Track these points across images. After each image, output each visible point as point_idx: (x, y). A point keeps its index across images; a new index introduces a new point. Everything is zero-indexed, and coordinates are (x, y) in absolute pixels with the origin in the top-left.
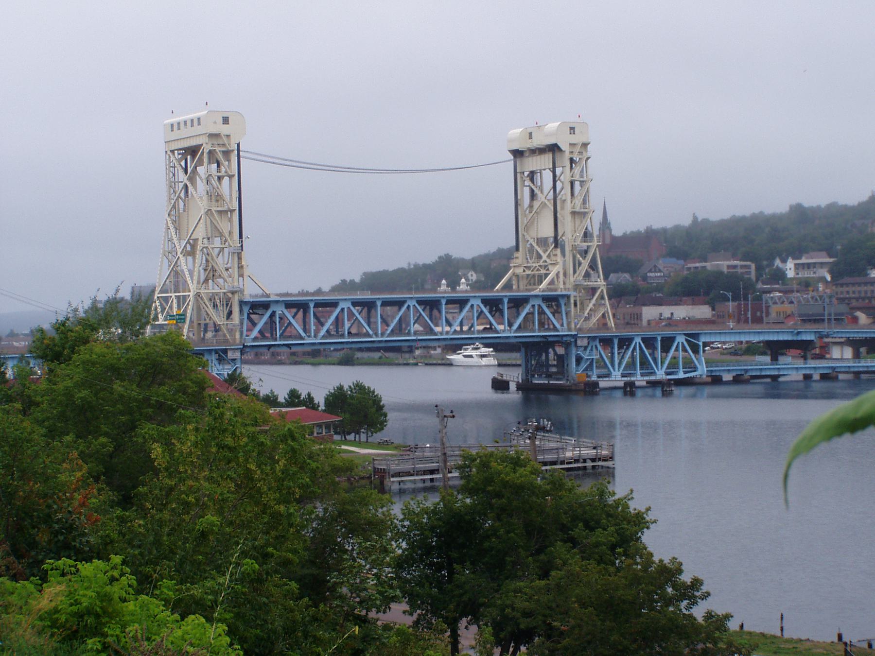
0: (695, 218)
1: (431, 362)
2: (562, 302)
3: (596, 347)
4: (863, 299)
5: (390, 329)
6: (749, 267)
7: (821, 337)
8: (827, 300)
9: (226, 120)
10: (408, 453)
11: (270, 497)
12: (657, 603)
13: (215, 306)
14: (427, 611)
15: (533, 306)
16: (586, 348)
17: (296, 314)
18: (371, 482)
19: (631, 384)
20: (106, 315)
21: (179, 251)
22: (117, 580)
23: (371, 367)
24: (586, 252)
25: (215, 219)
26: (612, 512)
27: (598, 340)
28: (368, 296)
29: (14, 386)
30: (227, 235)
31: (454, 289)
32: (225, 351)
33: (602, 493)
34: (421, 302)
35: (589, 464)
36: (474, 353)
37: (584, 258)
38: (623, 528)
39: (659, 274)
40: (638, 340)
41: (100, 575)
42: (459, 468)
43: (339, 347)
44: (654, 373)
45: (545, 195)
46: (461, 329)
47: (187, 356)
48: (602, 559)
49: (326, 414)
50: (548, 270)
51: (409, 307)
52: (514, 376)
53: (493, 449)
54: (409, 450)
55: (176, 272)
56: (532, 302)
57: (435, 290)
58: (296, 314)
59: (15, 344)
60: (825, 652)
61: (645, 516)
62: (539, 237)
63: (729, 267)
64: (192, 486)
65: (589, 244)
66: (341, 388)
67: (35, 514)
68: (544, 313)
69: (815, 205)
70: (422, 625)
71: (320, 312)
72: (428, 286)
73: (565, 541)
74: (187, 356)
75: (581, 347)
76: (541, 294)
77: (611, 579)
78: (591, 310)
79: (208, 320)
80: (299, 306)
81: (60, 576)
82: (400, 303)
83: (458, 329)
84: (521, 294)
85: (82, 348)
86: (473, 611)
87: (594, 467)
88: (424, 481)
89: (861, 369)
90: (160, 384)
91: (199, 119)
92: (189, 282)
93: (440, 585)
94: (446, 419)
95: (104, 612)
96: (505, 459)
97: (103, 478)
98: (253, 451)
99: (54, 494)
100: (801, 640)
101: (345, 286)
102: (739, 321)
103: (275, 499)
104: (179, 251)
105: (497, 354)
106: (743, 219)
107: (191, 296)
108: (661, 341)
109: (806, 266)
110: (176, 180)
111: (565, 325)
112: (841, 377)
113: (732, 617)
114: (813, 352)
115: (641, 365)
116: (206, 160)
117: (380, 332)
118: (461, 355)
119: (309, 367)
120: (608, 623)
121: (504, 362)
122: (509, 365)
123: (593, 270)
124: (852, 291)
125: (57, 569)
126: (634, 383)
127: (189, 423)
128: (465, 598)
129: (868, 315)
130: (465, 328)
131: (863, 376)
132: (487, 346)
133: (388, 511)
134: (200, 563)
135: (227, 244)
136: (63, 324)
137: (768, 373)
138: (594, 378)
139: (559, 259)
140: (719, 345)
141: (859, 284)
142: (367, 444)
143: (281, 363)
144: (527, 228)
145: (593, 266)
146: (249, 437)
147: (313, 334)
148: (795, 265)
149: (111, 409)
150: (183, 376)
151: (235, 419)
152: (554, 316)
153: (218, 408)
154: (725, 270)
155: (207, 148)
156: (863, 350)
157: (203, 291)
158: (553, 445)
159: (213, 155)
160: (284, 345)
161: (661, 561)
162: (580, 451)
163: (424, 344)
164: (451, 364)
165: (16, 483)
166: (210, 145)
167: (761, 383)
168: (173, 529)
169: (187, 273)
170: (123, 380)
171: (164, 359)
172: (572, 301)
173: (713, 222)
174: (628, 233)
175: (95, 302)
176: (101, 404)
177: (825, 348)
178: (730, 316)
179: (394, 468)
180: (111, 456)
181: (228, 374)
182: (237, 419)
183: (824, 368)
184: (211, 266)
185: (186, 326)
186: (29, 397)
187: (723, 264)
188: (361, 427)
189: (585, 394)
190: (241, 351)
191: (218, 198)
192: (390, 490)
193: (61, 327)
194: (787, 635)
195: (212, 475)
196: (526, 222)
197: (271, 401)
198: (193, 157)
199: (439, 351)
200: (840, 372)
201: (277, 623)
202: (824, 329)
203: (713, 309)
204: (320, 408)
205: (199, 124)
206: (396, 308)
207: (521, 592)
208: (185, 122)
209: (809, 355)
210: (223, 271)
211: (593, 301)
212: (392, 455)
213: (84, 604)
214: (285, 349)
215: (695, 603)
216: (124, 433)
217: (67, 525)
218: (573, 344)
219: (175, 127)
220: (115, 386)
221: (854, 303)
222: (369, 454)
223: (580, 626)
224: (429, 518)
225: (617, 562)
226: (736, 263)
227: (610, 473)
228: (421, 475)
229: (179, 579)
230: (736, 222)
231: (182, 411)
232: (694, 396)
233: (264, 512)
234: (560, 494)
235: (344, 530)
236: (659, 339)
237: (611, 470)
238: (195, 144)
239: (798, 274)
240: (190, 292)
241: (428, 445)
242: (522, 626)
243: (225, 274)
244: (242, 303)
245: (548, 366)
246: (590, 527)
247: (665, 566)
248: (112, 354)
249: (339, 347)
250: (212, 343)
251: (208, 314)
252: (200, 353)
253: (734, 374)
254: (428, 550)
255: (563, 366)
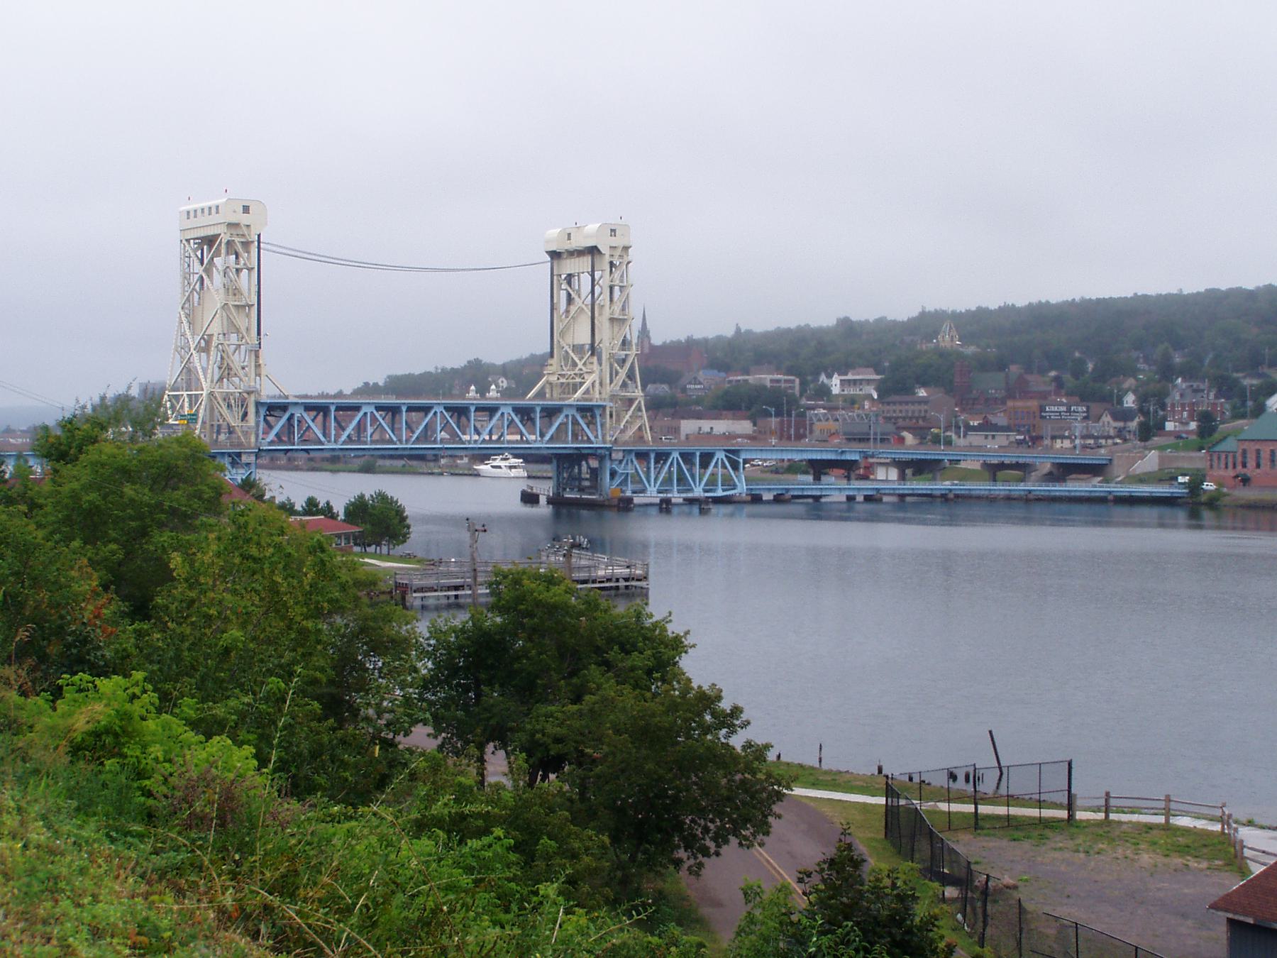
0: (738, 330)
1: (457, 472)
2: (598, 412)
3: (632, 461)
4: (911, 418)
5: (415, 436)
6: (793, 382)
7: (866, 458)
8: (873, 419)
9: (246, 209)
10: (432, 567)
11: (296, 612)
12: (694, 731)
13: (229, 406)
14: (452, 734)
15: (567, 416)
16: (621, 462)
17: (315, 417)
18: (392, 597)
19: (667, 502)
20: (117, 413)
21: (192, 347)
22: (139, 698)
23: (390, 475)
24: (624, 361)
25: (233, 314)
26: (649, 635)
27: (634, 454)
28: (392, 400)
29: (14, 486)
30: (243, 330)
31: (483, 396)
32: (239, 455)
33: (639, 615)
34: (448, 408)
35: (622, 584)
36: (503, 464)
37: (622, 367)
38: (660, 653)
39: (699, 386)
40: (676, 455)
41: (120, 692)
42: (490, 585)
43: (360, 453)
44: (691, 490)
45: (582, 301)
46: (491, 438)
47: (204, 460)
48: (637, 685)
49: (345, 524)
50: (583, 378)
51: (435, 413)
52: (545, 489)
53: (526, 566)
54: (433, 565)
55: (188, 370)
56: (565, 412)
57: (462, 396)
58: (315, 417)
59: (11, 440)
60: (865, 785)
61: (683, 640)
62: (575, 343)
63: (772, 381)
64: (214, 598)
65: (628, 353)
66: (362, 497)
67: (47, 625)
68: (579, 424)
69: (863, 319)
70: (447, 749)
71: (340, 416)
72: (455, 392)
73: (599, 664)
74: (204, 460)
75: (616, 460)
76: (575, 403)
77: (647, 704)
78: (627, 422)
79: (221, 420)
80: (319, 409)
81: (77, 692)
82: (426, 409)
83: (487, 438)
84: (553, 403)
85: (91, 448)
86: (500, 735)
87: (627, 587)
88: (448, 597)
89: (906, 492)
90: (174, 489)
91: (217, 207)
92: (203, 380)
93: (466, 708)
94: (477, 533)
95: (124, 732)
96: (537, 577)
97: (113, 587)
98: (280, 563)
99: (68, 604)
100: (840, 772)
101: (368, 389)
102: (781, 439)
103: (302, 615)
104: (192, 347)
105: (528, 465)
106: (789, 331)
107: (204, 395)
108: (700, 456)
109: (852, 383)
110: (192, 271)
111: (600, 437)
112: (885, 499)
113: (772, 747)
114: (857, 472)
115: (678, 480)
116: (223, 251)
117: (404, 439)
118: (489, 466)
119: (328, 474)
120: (644, 752)
121: (534, 474)
122: (539, 478)
123: (631, 380)
124: (896, 410)
125: (73, 685)
126: (670, 501)
127: (212, 531)
128: (493, 722)
129: (914, 435)
130: (494, 437)
131: (908, 499)
132: (516, 456)
133: (412, 629)
134: (223, 681)
135: (244, 341)
136: (70, 422)
137: (809, 493)
138: (629, 494)
139: (596, 367)
140: (760, 463)
141: (907, 403)
142: (388, 557)
143: (297, 469)
144: (562, 334)
145: (631, 376)
146: (275, 547)
147: (333, 439)
148: (841, 380)
149: (121, 514)
150: (199, 480)
151: (260, 528)
152: (588, 427)
153: (242, 516)
154: (768, 384)
155: (225, 238)
156: (909, 472)
157: (217, 390)
158: (583, 562)
159: (232, 246)
160: (302, 450)
161: (700, 687)
162: (613, 570)
163: (449, 452)
164: (478, 475)
165: (26, 591)
166: (229, 235)
167: (802, 503)
168: (193, 644)
169: (200, 371)
170: (134, 483)
171: (179, 462)
172: (608, 413)
173: (756, 333)
174: (668, 342)
175: (103, 398)
176: (110, 508)
177: (870, 469)
178: (772, 433)
179: (417, 582)
180: (120, 564)
181: (242, 479)
182: (263, 528)
183: (867, 489)
184: (226, 365)
185: (198, 426)
186: (32, 499)
187: (766, 378)
188: (382, 539)
189: (619, 511)
190: (256, 456)
191: (236, 291)
192: (412, 606)
193: (69, 425)
194: (825, 767)
195: (235, 587)
196: (561, 327)
197: (288, 508)
198: (210, 247)
199: (466, 460)
200: (885, 494)
201: (302, 746)
202: (870, 448)
203: (755, 425)
204: (339, 518)
205: (217, 212)
206: (422, 414)
207: (552, 716)
208: (203, 210)
209: (853, 476)
210: (239, 369)
211: (630, 413)
212: (417, 570)
213: (103, 723)
214: (304, 455)
215: (734, 732)
216: (134, 539)
217: (81, 638)
218: (607, 458)
219: (192, 214)
220: (125, 490)
221: (901, 423)
222: (393, 567)
223: (613, 754)
224: (457, 637)
225: (653, 687)
226: (779, 377)
227: (644, 594)
228: (445, 591)
229: (200, 697)
230: (781, 334)
231: (204, 519)
232: (732, 515)
233: (289, 628)
234: (595, 614)
235: (365, 647)
236: (698, 454)
237: (644, 591)
238: (212, 233)
239: (843, 391)
240: (203, 390)
241: (453, 560)
242: (552, 753)
243: (241, 373)
244: (258, 404)
245: (580, 479)
246: (626, 650)
247: (704, 693)
248: (124, 456)
249: (360, 453)
250: (226, 446)
251: (221, 415)
252: (213, 457)
253: (775, 493)
254: (455, 671)
255: (597, 481)
